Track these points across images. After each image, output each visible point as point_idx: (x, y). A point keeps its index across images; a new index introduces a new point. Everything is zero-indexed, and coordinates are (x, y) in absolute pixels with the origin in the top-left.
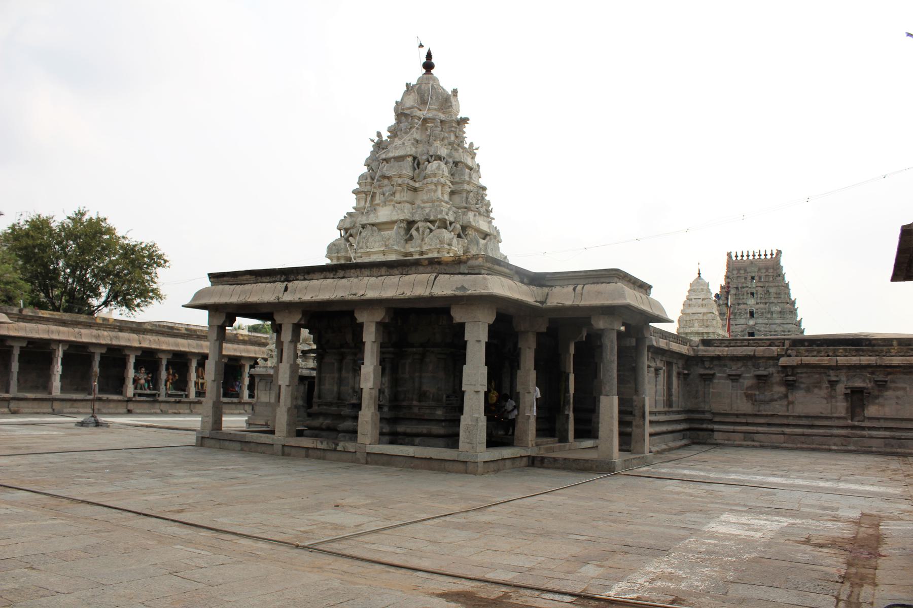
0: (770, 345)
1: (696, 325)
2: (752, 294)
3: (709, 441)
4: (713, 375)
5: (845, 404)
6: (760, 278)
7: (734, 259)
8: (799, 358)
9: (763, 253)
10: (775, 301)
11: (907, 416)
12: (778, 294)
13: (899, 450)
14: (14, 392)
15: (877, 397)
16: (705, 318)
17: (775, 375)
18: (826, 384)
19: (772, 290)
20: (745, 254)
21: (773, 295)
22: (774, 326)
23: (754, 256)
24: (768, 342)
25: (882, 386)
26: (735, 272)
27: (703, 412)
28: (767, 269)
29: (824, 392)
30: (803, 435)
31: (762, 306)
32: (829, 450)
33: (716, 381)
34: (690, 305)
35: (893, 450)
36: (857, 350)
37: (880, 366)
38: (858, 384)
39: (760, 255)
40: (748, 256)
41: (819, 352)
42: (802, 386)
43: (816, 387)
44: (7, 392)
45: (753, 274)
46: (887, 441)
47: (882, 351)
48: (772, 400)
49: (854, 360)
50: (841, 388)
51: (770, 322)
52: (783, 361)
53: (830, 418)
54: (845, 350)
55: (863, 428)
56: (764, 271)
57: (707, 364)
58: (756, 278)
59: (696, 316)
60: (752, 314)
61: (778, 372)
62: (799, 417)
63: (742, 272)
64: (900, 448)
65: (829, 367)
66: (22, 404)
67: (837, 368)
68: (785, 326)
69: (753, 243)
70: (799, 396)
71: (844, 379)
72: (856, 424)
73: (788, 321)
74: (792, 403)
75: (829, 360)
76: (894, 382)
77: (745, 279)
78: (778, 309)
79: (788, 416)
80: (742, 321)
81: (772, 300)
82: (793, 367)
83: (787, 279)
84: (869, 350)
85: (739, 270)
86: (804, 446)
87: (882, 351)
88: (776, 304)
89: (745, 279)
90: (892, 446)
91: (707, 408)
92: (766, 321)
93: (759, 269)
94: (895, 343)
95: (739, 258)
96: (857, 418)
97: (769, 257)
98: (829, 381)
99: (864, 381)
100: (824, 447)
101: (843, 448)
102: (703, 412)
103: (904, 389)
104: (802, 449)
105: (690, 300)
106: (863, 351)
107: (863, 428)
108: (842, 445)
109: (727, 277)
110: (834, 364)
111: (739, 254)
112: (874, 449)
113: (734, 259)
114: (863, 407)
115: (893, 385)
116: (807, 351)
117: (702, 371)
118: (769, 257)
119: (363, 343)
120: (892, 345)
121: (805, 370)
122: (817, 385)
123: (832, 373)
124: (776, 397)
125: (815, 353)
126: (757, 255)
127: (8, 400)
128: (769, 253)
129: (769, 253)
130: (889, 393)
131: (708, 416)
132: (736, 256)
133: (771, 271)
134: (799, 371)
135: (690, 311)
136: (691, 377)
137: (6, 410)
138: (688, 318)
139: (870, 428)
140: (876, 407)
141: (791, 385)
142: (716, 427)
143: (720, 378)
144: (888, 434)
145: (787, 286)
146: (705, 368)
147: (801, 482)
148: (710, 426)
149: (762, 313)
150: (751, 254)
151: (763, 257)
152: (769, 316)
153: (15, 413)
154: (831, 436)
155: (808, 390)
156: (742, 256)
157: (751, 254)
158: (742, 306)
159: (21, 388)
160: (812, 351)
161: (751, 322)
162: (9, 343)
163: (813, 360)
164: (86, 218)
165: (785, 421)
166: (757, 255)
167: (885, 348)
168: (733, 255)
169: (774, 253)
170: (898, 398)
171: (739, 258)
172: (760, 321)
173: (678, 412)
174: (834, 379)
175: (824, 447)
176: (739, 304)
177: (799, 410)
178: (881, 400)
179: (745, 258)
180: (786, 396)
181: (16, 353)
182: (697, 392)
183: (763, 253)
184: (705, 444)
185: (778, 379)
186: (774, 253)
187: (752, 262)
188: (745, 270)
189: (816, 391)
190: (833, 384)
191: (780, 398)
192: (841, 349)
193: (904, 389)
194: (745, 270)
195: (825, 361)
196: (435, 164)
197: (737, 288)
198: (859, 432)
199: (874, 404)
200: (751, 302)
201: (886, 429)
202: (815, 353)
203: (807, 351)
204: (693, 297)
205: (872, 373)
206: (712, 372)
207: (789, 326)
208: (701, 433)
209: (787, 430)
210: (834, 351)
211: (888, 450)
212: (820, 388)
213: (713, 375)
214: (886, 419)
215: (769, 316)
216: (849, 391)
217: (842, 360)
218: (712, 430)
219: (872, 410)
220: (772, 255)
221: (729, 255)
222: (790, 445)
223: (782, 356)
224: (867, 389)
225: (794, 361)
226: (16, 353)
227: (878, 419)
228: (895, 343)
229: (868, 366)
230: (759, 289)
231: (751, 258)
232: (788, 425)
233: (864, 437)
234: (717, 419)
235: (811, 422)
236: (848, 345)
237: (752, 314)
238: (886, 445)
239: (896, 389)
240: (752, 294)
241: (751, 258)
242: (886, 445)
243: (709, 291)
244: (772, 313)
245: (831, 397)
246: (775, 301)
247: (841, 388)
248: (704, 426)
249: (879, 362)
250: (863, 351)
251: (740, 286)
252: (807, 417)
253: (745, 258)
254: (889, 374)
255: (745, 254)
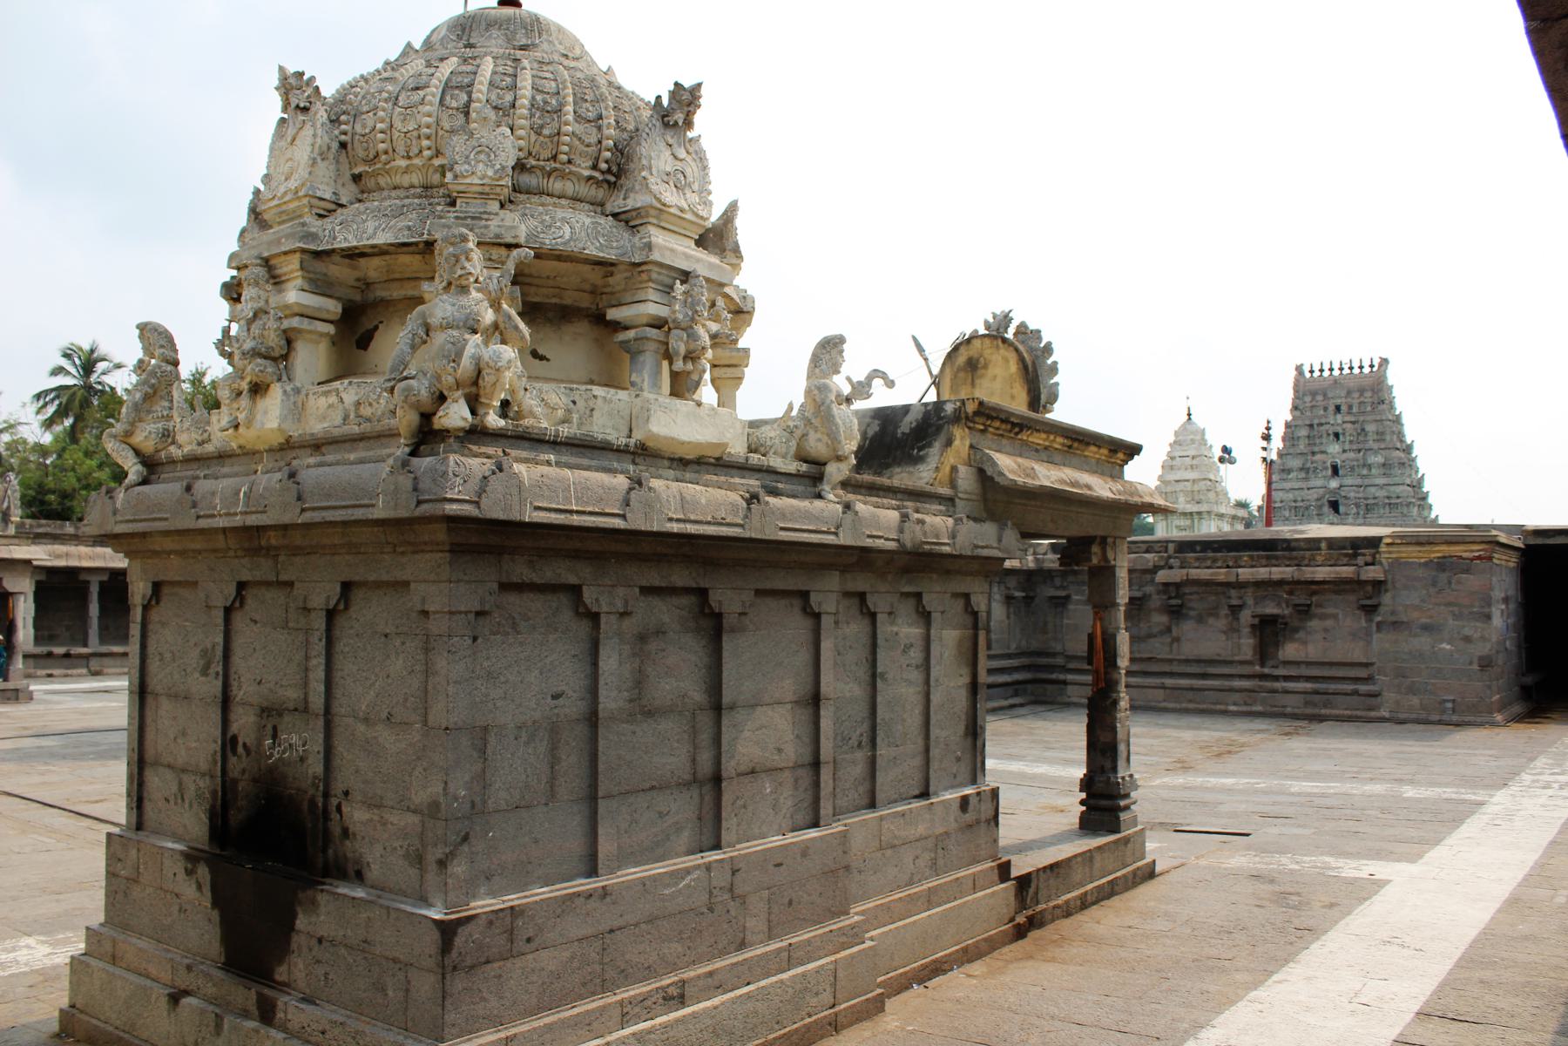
0: (1147, 551)
1: (1181, 499)
2: (1337, 435)
3: (1059, 699)
4: (1068, 597)
5: (1251, 641)
6: (1350, 407)
7: (1308, 375)
8: (1184, 571)
9: (1356, 365)
10: (1375, 446)
11: (1338, 658)
12: (1380, 436)
13: (1323, 711)
14: (94, 645)
15: (1296, 630)
16: (1196, 488)
17: (1155, 597)
18: (1225, 611)
19: (1370, 428)
20: (1326, 367)
21: (1371, 437)
22: (1373, 490)
23: (1341, 369)
24: (1144, 546)
25: (1304, 612)
26: (1308, 399)
27: (1054, 655)
28: (1362, 391)
29: (1222, 623)
30: (1192, 689)
31: (1352, 455)
32: (1225, 713)
33: (1071, 607)
34: (1172, 468)
35: (1316, 711)
36: (1268, 558)
37: (1299, 582)
38: (1270, 609)
39: (1351, 368)
40: (1331, 370)
41: (1215, 560)
42: (1192, 613)
43: (1211, 615)
44: (85, 645)
45: (1338, 401)
46: (1309, 697)
47: (1303, 558)
48: (1150, 636)
49: (1262, 573)
50: (1246, 616)
51: (1367, 482)
52: (1162, 576)
53: (1231, 662)
54: (1251, 557)
55: (1276, 678)
56: (1356, 395)
57: (1058, 581)
58: (1344, 408)
59: (1181, 486)
60: (1335, 470)
61: (1159, 593)
62: (1187, 661)
63: (1320, 398)
64: (1325, 706)
65: (1228, 585)
66: (106, 661)
67: (1240, 585)
68: (1392, 488)
69: (1339, 348)
70: (1187, 628)
71: (1250, 602)
72: (1266, 671)
73: (1397, 480)
74: (1177, 640)
75: (1227, 574)
76: (1320, 606)
77: (1325, 409)
78: (1380, 459)
79: (1170, 661)
80: (1319, 483)
81: (1371, 444)
82: (1178, 585)
83: (1400, 406)
84: (1285, 557)
85: (1314, 394)
86: (1191, 706)
87: (1303, 558)
88: (1376, 452)
89: (1325, 409)
90: (1315, 705)
91: (1059, 648)
92: (1358, 481)
93: (1349, 393)
94: (1323, 545)
95: (1316, 374)
96: (1271, 663)
97: (1366, 370)
98: (1230, 606)
99: (1279, 604)
100: (1219, 707)
101: (1245, 708)
102: (1054, 655)
103: (1335, 617)
104: (1186, 711)
105: (1172, 458)
106: (1276, 558)
107: (1276, 678)
108: (1246, 704)
109: (1295, 408)
110: (1233, 579)
111: (1316, 368)
112: (1289, 710)
113: (1308, 375)
114: (1277, 645)
115: (1319, 611)
116: (1197, 559)
117: (1052, 592)
118: (1366, 370)
119: (1284, 439)
120: (1319, 549)
121: (1195, 589)
122: (1213, 612)
123: (1233, 593)
124: (1155, 630)
125: (1209, 563)
126: (1346, 367)
127: (87, 657)
128: (1366, 364)
129: (1366, 364)
130: (1314, 624)
131: (1060, 661)
132: (1312, 372)
133: (1369, 394)
134: (1187, 590)
135: (1172, 477)
136: (1037, 600)
137: (84, 671)
138: (1169, 489)
139: (1287, 678)
140: (1296, 645)
141: (1176, 613)
142: (1070, 677)
143: (1078, 603)
144: (1309, 686)
145: (1397, 420)
146: (1057, 588)
147: (1042, 769)
148: (1062, 677)
149: (1352, 468)
150: (1336, 366)
151: (1346, 371)
152: (1365, 472)
153: (96, 674)
154: (1231, 690)
155: (1200, 620)
156: (1321, 370)
157: (1336, 366)
158: (1318, 457)
159: (103, 640)
160: (1205, 559)
161: (1334, 484)
162: (83, 577)
163: (1204, 574)
164: (207, 380)
165: (1167, 668)
166: (1346, 367)
167: (1308, 553)
168: (1306, 369)
169: (1376, 363)
170: (1326, 630)
171: (1316, 374)
172: (1349, 481)
173: (1009, 656)
174: (1235, 602)
175: (1219, 707)
176: (1313, 453)
177: (1188, 650)
178: (1301, 634)
179: (1326, 374)
180: (1169, 630)
181: (94, 590)
182: (1046, 623)
183: (1356, 365)
184: (1052, 703)
185: (1158, 604)
186: (1376, 363)
187: (1335, 381)
188: (1325, 395)
189: (1211, 621)
190: (1235, 610)
191: (1162, 633)
192: (1245, 556)
193: (1335, 617)
194: (1325, 395)
195: (1221, 574)
196: (66, 456)
197: (1311, 426)
198: (1268, 684)
199: (1293, 640)
200: (1334, 448)
201: (1308, 679)
202: (1209, 563)
203: (1197, 559)
204: (1177, 454)
205: (1291, 593)
206: (1063, 593)
207: (1399, 489)
208: (1049, 687)
209: (1169, 682)
210: (1236, 559)
211: (1309, 711)
212: (1217, 616)
213: (1068, 597)
214: (1309, 664)
215: (1365, 472)
216: (1256, 621)
217: (1245, 573)
218: (1065, 683)
219: (1290, 650)
220: (1372, 366)
221: (1299, 369)
222: (1171, 705)
223: (1162, 568)
224: (1283, 617)
225: (1176, 575)
226: (94, 590)
227: (1297, 663)
228: (1323, 545)
229: (1281, 583)
230: (1349, 426)
231: (1336, 373)
232: (1172, 675)
233: (1274, 691)
234: (1071, 666)
235: (1204, 667)
236: (1257, 549)
237: (1335, 470)
238: (1307, 703)
239: (1323, 617)
240: (1337, 435)
241: (1336, 373)
242: (1307, 703)
243: (1203, 442)
244: (1370, 467)
245: (1233, 630)
246: (1375, 446)
247: (1246, 616)
248: (1054, 676)
249: (1297, 576)
250: (1276, 558)
251: (1316, 421)
252: (1199, 661)
253: (1326, 374)
254: (1314, 593)
255: (1326, 367)
